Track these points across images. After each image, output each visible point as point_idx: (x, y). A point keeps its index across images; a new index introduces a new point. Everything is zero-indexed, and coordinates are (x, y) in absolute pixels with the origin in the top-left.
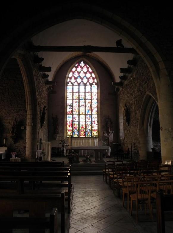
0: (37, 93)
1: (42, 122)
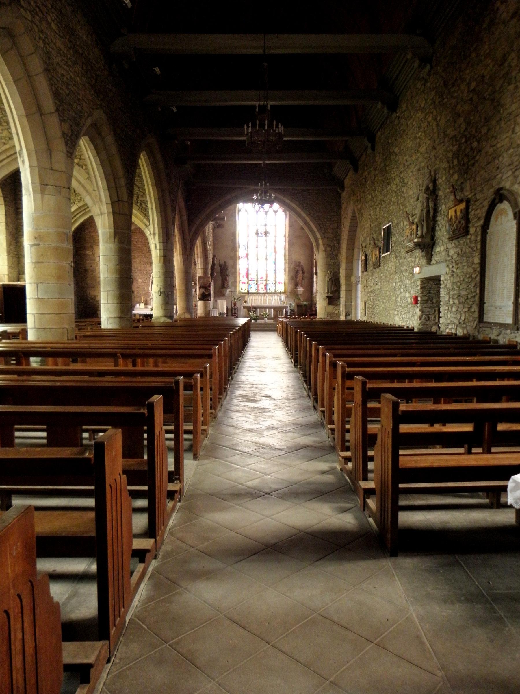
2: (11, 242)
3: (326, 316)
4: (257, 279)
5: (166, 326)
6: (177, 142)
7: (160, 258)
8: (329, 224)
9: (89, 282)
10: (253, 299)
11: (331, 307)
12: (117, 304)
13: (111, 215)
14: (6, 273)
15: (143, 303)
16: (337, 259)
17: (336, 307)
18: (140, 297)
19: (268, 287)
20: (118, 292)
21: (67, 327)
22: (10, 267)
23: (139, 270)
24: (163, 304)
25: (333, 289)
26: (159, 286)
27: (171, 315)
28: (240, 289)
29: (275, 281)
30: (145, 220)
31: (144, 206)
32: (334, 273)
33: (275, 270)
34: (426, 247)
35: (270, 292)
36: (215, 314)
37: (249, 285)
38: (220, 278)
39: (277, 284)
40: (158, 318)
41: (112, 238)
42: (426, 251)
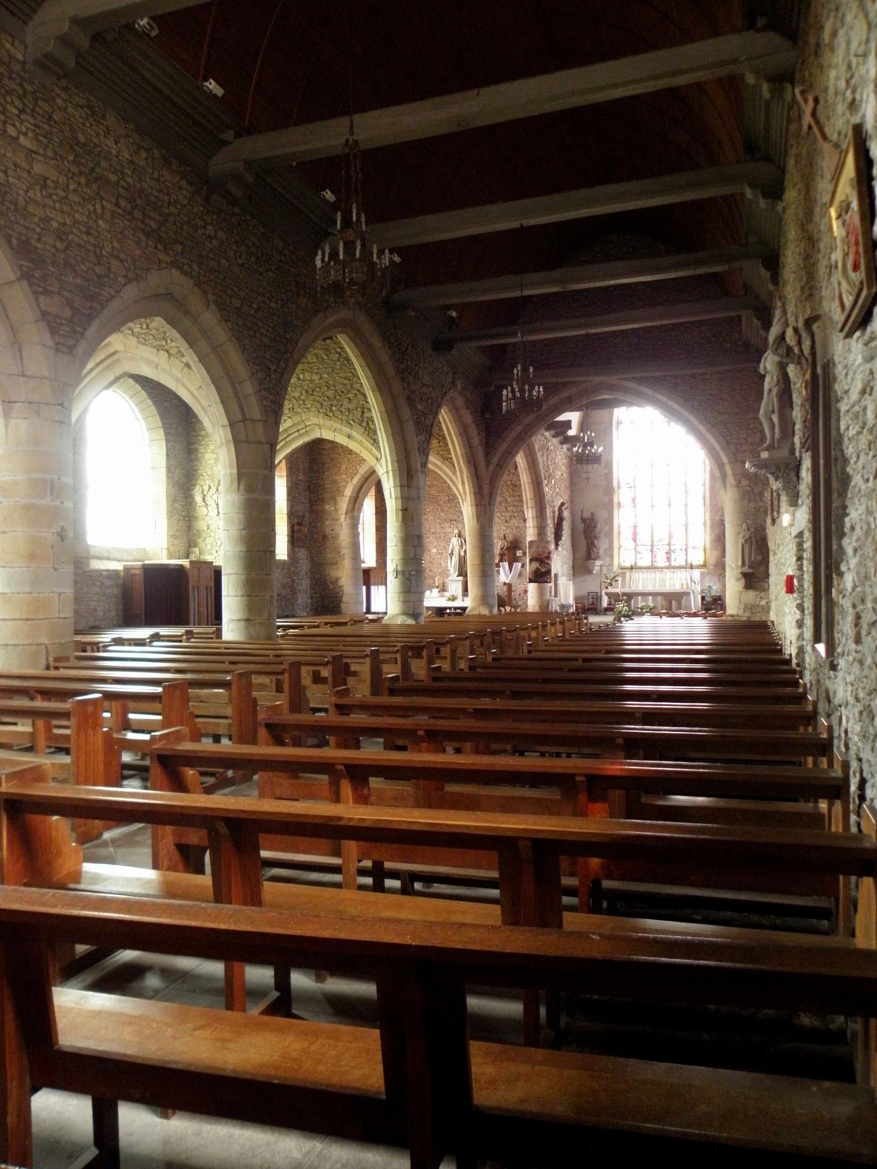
0: (545, 482)
1: (558, 537)
2: (176, 496)
3: (741, 612)
4: (652, 541)
5: (407, 631)
6: (413, 314)
7: (397, 514)
8: (745, 436)
9: (329, 555)
10: (641, 578)
11: (751, 595)
12: (242, 596)
13: (232, 445)
14: (165, 545)
15: (437, 587)
16: (762, 500)
17: (762, 594)
18: (433, 578)
19: (673, 556)
20: (244, 577)
21: (45, 641)
22: (172, 536)
23: (433, 533)
24: (401, 593)
25: (753, 559)
26: (395, 561)
27: (417, 611)
28: (621, 561)
29: (686, 545)
30: (374, 451)
31: (372, 427)
32: (756, 529)
33: (686, 525)
34: (782, 469)
35: (677, 565)
36: (555, 607)
37: (637, 552)
38: (584, 543)
39: (690, 551)
40: (393, 617)
41: (236, 484)
42: (783, 477)
